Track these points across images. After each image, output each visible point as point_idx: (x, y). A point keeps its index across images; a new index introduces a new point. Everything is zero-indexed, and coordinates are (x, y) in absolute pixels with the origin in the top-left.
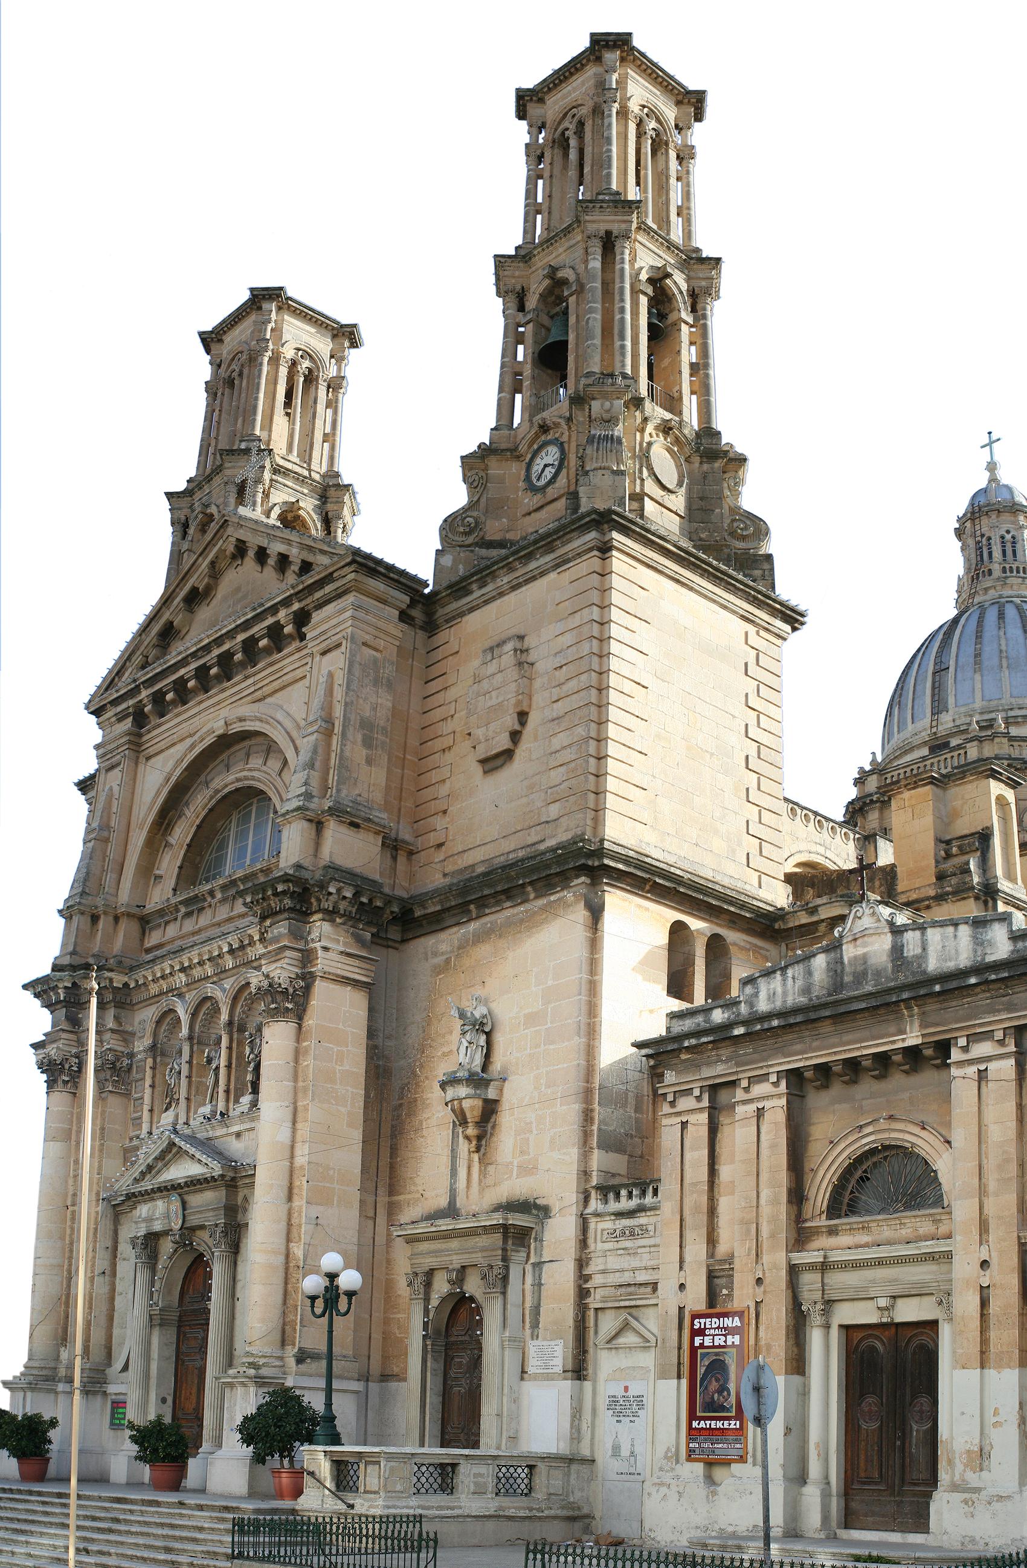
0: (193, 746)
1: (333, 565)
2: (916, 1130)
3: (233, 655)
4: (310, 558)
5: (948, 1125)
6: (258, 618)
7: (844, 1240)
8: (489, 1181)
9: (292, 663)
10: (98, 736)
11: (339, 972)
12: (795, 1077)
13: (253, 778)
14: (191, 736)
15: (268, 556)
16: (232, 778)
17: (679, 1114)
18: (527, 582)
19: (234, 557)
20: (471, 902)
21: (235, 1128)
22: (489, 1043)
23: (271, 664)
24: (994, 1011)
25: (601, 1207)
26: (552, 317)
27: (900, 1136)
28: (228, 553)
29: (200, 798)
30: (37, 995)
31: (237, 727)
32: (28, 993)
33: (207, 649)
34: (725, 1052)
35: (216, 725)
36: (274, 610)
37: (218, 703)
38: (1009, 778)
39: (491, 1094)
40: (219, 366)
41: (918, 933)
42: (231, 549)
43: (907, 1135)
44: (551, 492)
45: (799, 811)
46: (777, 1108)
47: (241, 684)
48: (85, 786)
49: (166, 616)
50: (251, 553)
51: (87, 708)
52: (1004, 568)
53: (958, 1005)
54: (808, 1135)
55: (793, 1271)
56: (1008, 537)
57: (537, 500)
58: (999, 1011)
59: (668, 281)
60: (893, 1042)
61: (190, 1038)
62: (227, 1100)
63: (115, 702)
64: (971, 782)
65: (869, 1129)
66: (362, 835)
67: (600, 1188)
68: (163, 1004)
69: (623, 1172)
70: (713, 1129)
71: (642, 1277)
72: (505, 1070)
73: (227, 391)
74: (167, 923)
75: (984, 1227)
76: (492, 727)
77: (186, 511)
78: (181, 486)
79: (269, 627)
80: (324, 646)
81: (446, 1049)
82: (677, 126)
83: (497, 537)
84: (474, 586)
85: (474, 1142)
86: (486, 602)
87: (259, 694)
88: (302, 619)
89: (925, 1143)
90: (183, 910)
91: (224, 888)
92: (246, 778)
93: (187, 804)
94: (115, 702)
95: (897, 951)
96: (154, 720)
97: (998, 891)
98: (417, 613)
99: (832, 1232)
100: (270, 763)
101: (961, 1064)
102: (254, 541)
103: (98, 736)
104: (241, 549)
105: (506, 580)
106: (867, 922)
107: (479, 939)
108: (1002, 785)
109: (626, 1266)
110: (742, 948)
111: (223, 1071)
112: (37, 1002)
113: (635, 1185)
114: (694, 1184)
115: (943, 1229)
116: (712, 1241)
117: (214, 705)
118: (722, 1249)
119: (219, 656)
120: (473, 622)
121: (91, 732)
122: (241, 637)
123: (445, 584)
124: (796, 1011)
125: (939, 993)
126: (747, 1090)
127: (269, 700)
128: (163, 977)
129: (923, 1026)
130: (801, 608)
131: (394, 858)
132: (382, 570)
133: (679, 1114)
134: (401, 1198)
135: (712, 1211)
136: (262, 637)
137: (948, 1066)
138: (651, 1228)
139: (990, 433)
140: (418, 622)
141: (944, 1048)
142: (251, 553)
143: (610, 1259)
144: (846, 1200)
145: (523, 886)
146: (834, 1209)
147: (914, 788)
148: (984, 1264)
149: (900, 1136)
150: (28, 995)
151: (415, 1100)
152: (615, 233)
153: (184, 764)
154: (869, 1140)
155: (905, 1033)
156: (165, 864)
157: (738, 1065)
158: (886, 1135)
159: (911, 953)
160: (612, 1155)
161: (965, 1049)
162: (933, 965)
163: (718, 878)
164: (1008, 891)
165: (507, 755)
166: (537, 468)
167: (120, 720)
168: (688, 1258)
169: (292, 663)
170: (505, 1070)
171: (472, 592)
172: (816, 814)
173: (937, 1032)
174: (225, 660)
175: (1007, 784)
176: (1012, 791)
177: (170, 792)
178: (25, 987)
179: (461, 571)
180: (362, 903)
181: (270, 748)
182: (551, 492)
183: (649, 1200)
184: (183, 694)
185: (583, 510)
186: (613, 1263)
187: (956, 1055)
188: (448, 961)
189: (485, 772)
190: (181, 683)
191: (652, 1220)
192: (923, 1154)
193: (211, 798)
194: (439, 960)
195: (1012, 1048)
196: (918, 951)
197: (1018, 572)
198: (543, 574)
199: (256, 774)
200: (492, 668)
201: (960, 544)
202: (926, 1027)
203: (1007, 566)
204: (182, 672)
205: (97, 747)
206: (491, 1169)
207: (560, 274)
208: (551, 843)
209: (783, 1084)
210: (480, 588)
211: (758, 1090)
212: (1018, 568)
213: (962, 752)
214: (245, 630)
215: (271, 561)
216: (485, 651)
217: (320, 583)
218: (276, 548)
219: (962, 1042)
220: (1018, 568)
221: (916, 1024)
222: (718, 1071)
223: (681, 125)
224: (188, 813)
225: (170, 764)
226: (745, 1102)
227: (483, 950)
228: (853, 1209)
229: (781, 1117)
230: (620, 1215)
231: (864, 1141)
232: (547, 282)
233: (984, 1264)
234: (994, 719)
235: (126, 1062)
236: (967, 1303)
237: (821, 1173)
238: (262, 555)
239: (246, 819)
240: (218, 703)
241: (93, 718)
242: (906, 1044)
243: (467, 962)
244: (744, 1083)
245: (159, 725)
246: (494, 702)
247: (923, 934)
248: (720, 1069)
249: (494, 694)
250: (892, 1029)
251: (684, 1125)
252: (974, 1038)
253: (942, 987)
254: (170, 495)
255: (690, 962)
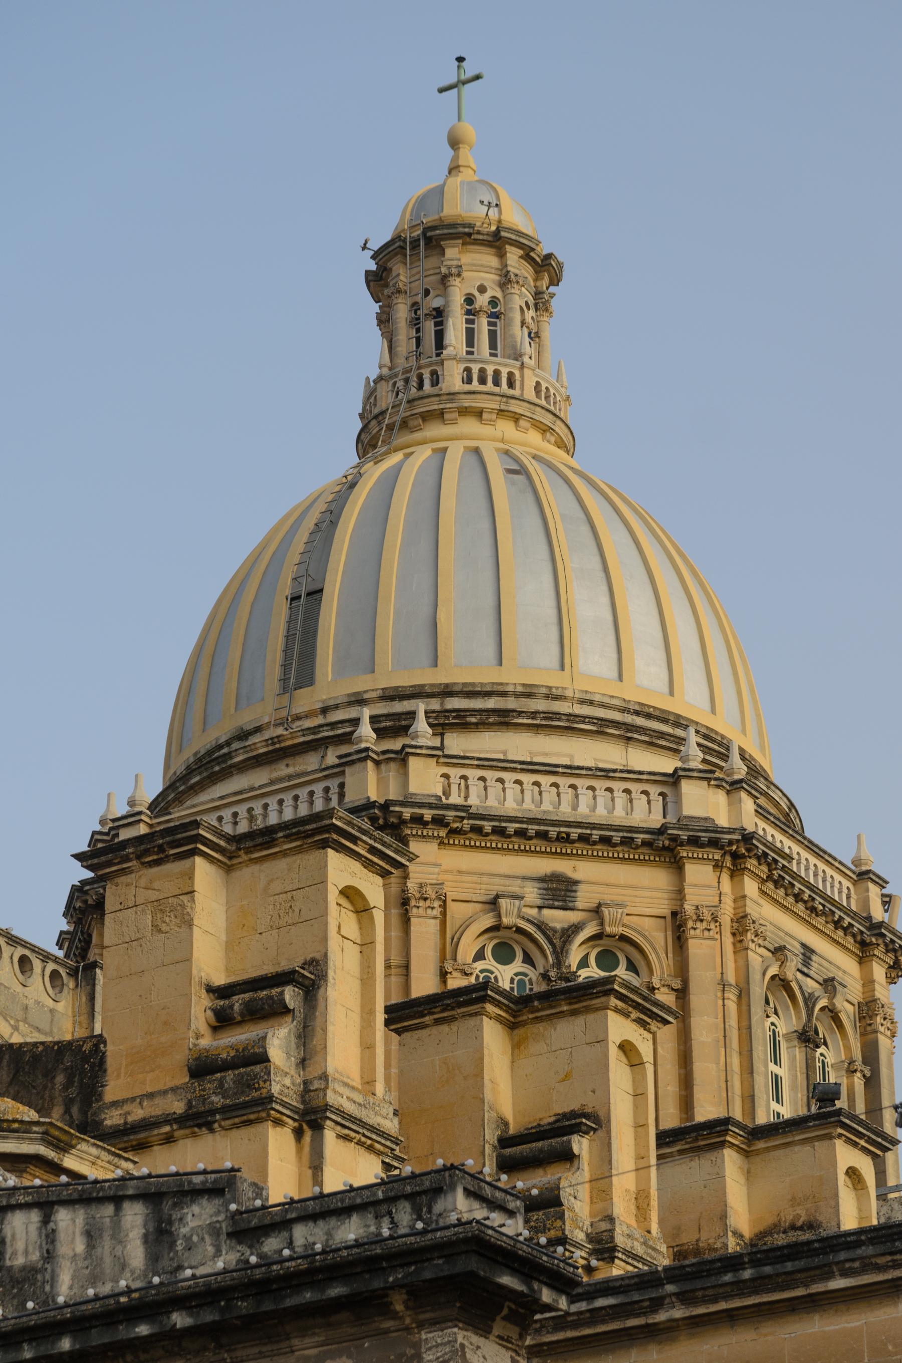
38: (372, 850)
41: (35, 1216)
52: (468, 370)
56: (482, 301)
64: (284, 854)
72: (376, 1178)
97: (326, 1107)
139: (460, 59)
147: (158, 863)
159: (20, 1261)
164: (349, 1108)
170: (345, 1185)
175: (368, 864)
176: (379, 880)
197: (497, 383)
201: (376, 308)
203: (475, 368)
212: (497, 374)
213: (333, 784)
220: (497, 374)
234: (412, 715)
247: (46, 1220)
253: (73, 1343)
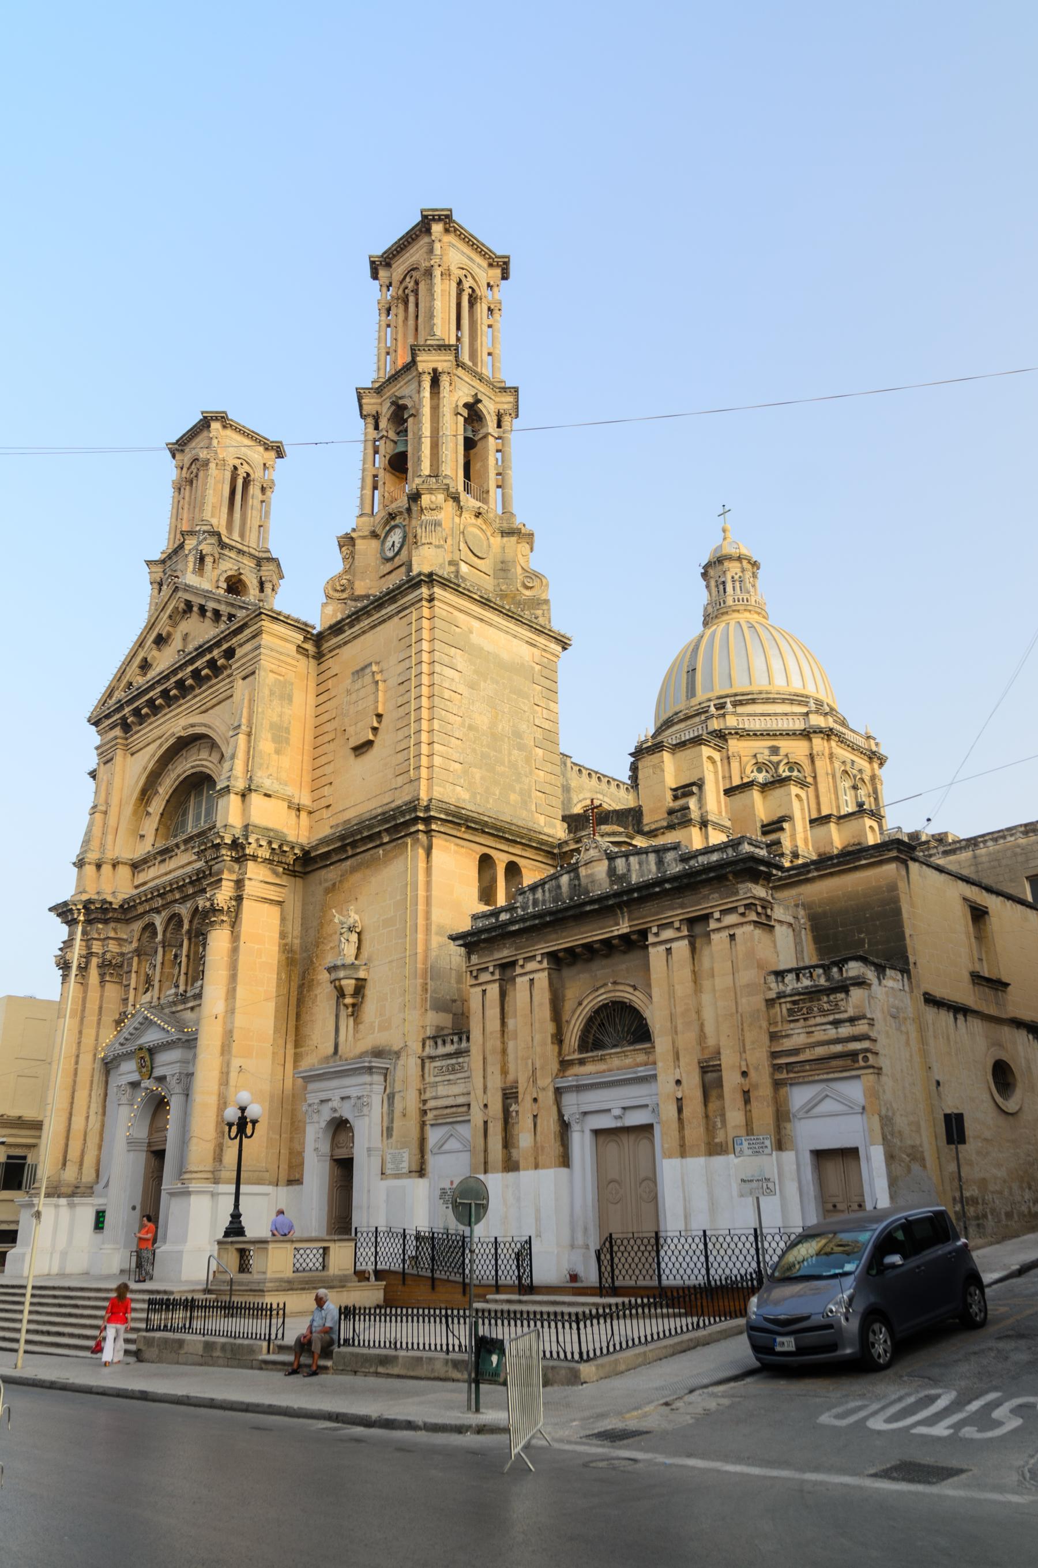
0: (161, 745)
1: (248, 616)
2: (631, 990)
3: (185, 681)
4: (233, 611)
5: (649, 985)
6: (200, 655)
7: (589, 1068)
8: (359, 1036)
9: (224, 686)
10: (97, 740)
11: (259, 894)
12: (552, 956)
13: (203, 766)
14: (160, 738)
15: (206, 611)
16: (188, 766)
17: (480, 984)
18: (380, 623)
19: (185, 612)
20: (347, 844)
21: (190, 1004)
22: (360, 940)
23: (211, 687)
24: (673, 909)
25: (433, 1053)
26: (398, 434)
27: (622, 994)
28: (180, 609)
29: (168, 780)
30: (59, 915)
31: (191, 731)
32: (52, 913)
33: (167, 678)
34: (508, 942)
35: (175, 730)
36: (210, 649)
37: (177, 715)
39: (362, 974)
40: (182, 468)
41: (624, 859)
42: (182, 606)
43: (626, 994)
44: (397, 561)
45: (593, 775)
46: (542, 979)
47: (192, 702)
48: (93, 775)
49: (141, 655)
50: (195, 609)
51: (89, 721)
53: (650, 907)
54: (564, 996)
55: (558, 1092)
57: (389, 567)
58: (676, 908)
59: (480, 405)
60: (612, 931)
61: (163, 942)
62: (186, 985)
63: (107, 716)
65: (602, 991)
66: (272, 801)
67: (434, 1038)
68: (146, 919)
69: (450, 1026)
70: (503, 994)
71: (461, 1100)
73: (188, 488)
74: (149, 867)
75: (677, 1056)
76: (360, 725)
77: (161, 575)
78: (157, 556)
79: (207, 661)
80: (243, 674)
81: (332, 945)
82: (489, 285)
83: (363, 593)
84: (346, 628)
85: (350, 1009)
86: (355, 638)
87: (203, 708)
88: (230, 653)
89: (637, 999)
90: (159, 859)
91: (186, 842)
92: (198, 766)
93: (160, 784)
94: (107, 716)
95: (612, 872)
96: (135, 729)
98: (309, 646)
99: (582, 1062)
100: (213, 754)
101: (654, 944)
102: (197, 601)
103: (97, 740)
104: (189, 605)
105: (367, 622)
106: (593, 853)
107: (353, 870)
108: (711, 750)
109: (450, 1093)
110: (530, 870)
111: (183, 965)
112: (59, 920)
113: (455, 1034)
114: (491, 1033)
115: (651, 1058)
116: (504, 1072)
117: (174, 717)
118: (511, 1077)
119: (192, 672)
120: (347, 652)
121: (92, 737)
122: (190, 668)
123: (327, 626)
124: (550, 913)
125: (638, 898)
126: (522, 966)
127: (210, 712)
128: (146, 901)
129: (630, 920)
130: (568, 635)
131: (298, 817)
132: (282, 618)
133: (480, 984)
134: (303, 1049)
135: (504, 1052)
136: (203, 669)
137: (647, 947)
138: (465, 1065)
140: (311, 653)
141: (644, 934)
142: (195, 609)
143: (440, 1088)
144: (591, 1041)
145: (380, 832)
146: (585, 1045)
148: (678, 1082)
149: (622, 994)
150: (53, 915)
151: (313, 980)
152: (440, 370)
153: (156, 758)
154: (602, 997)
155: (618, 924)
156: (146, 827)
157: (516, 950)
158: (612, 994)
160: (442, 1015)
161: (657, 934)
162: (634, 879)
163: (515, 821)
165: (369, 744)
166: (389, 544)
167: (111, 729)
168: (489, 1085)
169: (224, 686)
171: (345, 631)
172: (596, 773)
173: (639, 924)
174: (180, 684)
177: (148, 777)
178: (51, 910)
179: (339, 617)
180: (273, 849)
181: (213, 745)
182: (397, 561)
183: (464, 1045)
184: (155, 709)
185: (414, 573)
186: (442, 1090)
187: (651, 939)
188: (334, 885)
189: (356, 756)
190: (151, 703)
191: (466, 1059)
192: (636, 1006)
193: (176, 780)
194: (329, 884)
195: (686, 933)
196: (625, 871)
198: (390, 618)
199: (204, 763)
200: (357, 686)
202: (633, 920)
204: (151, 694)
205: (97, 748)
206: (361, 1026)
207: (401, 402)
208: (398, 802)
209: (545, 962)
210: (350, 628)
211: (531, 966)
214: (192, 664)
215: (209, 614)
216: (353, 674)
217: (240, 630)
218: (211, 605)
219: (655, 930)
221: (626, 919)
222: (504, 953)
223: (492, 283)
224: (161, 790)
225: (148, 757)
226: (521, 975)
227: (357, 876)
228: (598, 1045)
229: (545, 983)
230: (449, 1056)
231: (600, 999)
232: (393, 408)
233: (678, 1082)
235: (120, 959)
236: (669, 1111)
237: (573, 1022)
238: (203, 610)
239: (200, 793)
240: (177, 715)
241: (93, 727)
242: (620, 932)
243: (346, 885)
244: (521, 962)
245: (139, 731)
246: (360, 708)
247: (627, 860)
248: (505, 953)
249: (360, 702)
250: (611, 923)
251: (484, 991)
252: (662, 927)
254: (149, 563)
255: (494, 880)
